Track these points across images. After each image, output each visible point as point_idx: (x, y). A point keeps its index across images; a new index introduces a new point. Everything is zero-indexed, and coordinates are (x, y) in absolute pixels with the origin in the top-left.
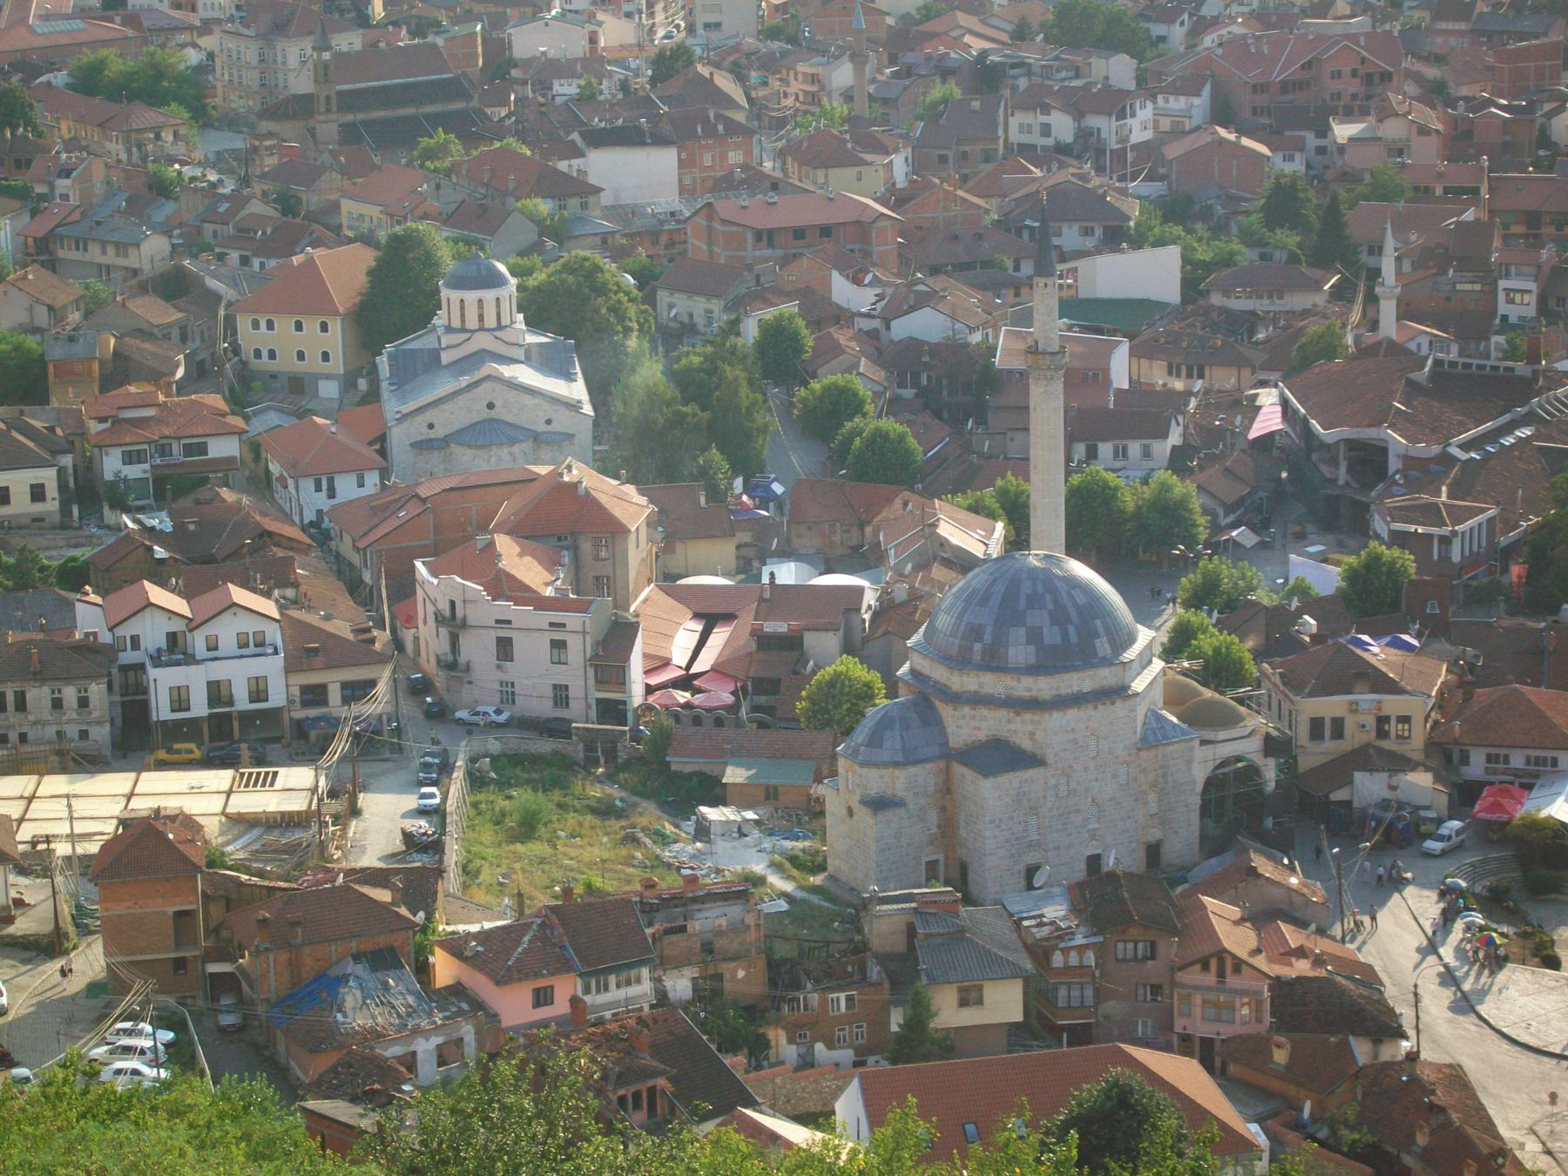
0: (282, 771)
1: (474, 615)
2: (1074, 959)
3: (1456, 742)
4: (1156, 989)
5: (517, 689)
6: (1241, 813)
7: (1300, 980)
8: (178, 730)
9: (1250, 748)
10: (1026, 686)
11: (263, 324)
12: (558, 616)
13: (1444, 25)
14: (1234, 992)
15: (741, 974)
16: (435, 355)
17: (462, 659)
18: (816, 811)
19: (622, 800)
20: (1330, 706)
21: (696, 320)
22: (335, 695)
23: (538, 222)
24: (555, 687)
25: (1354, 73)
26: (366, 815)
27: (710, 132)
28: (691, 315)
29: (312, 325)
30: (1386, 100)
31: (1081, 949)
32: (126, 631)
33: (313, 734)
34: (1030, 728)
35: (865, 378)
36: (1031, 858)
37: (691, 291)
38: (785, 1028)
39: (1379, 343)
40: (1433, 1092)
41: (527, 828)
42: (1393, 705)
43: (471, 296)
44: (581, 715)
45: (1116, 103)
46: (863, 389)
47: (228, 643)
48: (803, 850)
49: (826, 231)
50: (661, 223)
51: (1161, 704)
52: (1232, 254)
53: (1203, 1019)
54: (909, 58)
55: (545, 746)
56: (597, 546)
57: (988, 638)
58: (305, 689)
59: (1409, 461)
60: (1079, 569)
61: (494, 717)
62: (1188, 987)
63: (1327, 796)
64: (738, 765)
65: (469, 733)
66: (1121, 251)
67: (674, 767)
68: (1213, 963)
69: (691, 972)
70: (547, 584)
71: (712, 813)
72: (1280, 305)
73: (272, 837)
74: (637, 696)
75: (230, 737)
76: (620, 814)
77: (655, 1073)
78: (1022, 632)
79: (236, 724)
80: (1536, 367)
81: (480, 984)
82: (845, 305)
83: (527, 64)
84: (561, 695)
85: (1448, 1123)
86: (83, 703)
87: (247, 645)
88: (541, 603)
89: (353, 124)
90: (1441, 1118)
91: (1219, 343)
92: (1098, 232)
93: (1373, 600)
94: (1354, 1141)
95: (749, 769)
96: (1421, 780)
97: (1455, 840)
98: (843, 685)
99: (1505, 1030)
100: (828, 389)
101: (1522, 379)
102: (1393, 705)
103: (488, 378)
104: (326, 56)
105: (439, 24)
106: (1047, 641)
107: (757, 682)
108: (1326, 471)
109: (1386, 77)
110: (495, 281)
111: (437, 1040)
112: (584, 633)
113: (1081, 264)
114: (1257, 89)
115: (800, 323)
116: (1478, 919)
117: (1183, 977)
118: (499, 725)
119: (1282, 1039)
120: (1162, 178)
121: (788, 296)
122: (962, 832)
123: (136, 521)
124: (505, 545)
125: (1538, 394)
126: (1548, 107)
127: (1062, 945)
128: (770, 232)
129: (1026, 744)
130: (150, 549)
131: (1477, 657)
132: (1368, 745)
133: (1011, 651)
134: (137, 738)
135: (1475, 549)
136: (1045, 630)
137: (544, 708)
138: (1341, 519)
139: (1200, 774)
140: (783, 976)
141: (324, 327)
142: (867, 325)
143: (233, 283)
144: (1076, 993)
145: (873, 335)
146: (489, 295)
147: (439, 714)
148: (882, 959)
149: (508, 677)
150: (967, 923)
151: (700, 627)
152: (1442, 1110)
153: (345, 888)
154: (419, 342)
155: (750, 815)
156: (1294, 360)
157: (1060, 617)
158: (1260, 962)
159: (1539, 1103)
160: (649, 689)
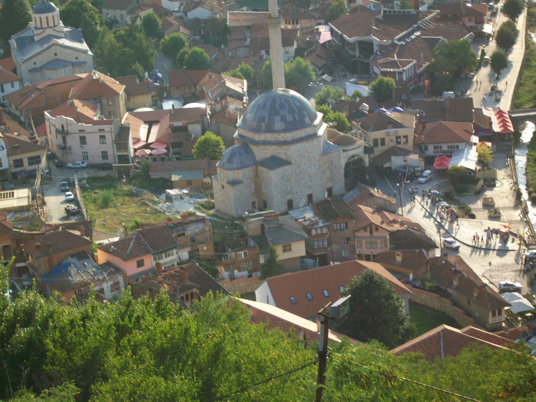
1: (71, 129)
2: (319, 231)
3: (423, 143)
4: (348, 239)
5: (89, 154)
6: (358, 175)
7: (398, 231)
9: (359, 152)
10: (282, 137)
14: (377, 238)
15: (205, 248)
16: (32, 38)
17: (68, 146)
19: (136, 190)
20: (379, 134)
21: (117, 17)
22: (26, 162)
24: (102, 152)
26: (48, 204)
28: (115, 17)
31: (321, 228)
33: (19, 177)
34: (285, 151)
36: (289, 197)
37: (114, 8)
38: (224, 266)
39: (358, 7)
40: (455, 266)
41: (105, 204)
42: (401, 132)
43: (43, 16)
46: (184, 38)
48: (205, 202)
51: (327, 138)
53: (366, 248)
55: (103, 173)
56: (108, 100)
57: (267, 121)
59: (381, 47)
61: (82, 165)
62: (360, 237)
63: (382, 166)
64: (175, 174)
65: (76, 171)
67: (152, 177)
68: (368, 229)
69: (188, 249)
70: (94, 116)
71: (172, 192)
73: (18, 215)
74: (132, 154)
76: (137, 195)
77: (192, 287)
80: (418, 10)
81: (117, 261)
82: (168, 8)
84: (105, 155)
85: (463, 276)
88: (95, 123)
90: (460, 275)
91: (302, 11)
93: (382, 96)
94: (431, 286)
95: (179, 175)
96: (414, 158)
97: (429, 177)
98: (209, 142)
99: (464, 242)
100: (172, 39)
101: (413, 15)
102: (401, 132)
103: (54, 44)
106: (288, 120)
107: (173, 144)
108: (351, 53)
110: (52, 9)
111: (110, 283)
112: (111, 132)
115: (156, 16)
116: (446, 204)
117: (358, 234)
118: (84, 168)
119: (399, 253)
121: (149, 7)
122: (264, 190)
124: (77, 103)
125: (420, 20)
127: (315, 227)
129: (284, 157)
131: (423, 113)
132: (394, 147)
133: (276, 125)
135: (410, 75)
136: (287, 116)
139: (343, 162)
140: (220, 248)
144: (321, 243)
145: (181, 18)
146: (50, 15)
147: (61, 166)
148: (254, 238)
149: (85, 150)
150: (282, 222)
152: (460, 272)
153: (64, 232)
155: (185, 191)
157: (291, 111)
158: (384, 226)
159: (483, 266)
160: (135, 150)
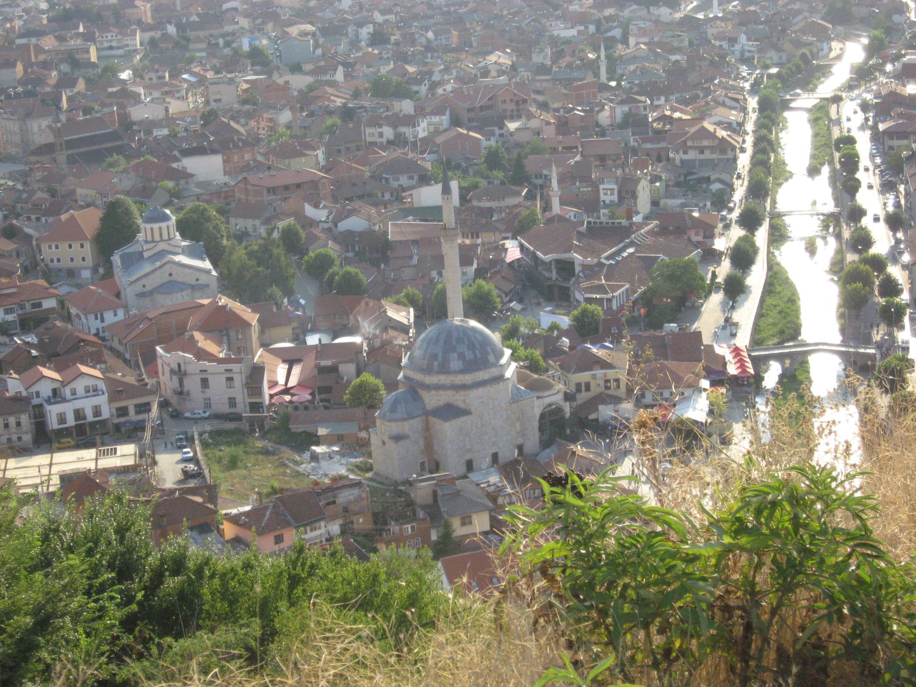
0: (119, 448)
1: (190, 369)
8: (61, 433)
9: (558, 398)
11: (54, 247)
12: (229, 366)
13: (540, 78)
15: (361, 520)
16: (141, 254)
17: (185, 390)
18: (366, 444)
20: (584, 377)
22: (132, 410)
23: (169, 191)
25: (511, 100)
26: (159, 464)
27: (236, 146)
29: (76, 245)
30: (529, 111)
32: (34, 389)
33: (123, 430)
34: (463, 398)
35: (332, 249)
41: (233, 463)
42: (611, 374)
43: (156, 226)
44: (241, 407)
45: (411, 121)
47: (81, 391)
49: (298, 186)
50: (221, 188)
52: (477, 183)
54: (313, 107)
55: (231, 426)
56: (237, 332)
58: (118, 409)
59: (585, 267)
60: (473, 323)
61: (203, 415)
64: (322, 427)
65: (196, 423)
66: (431, 185)
71: (318, 449)
72: (503, 204)
73: (122, 477)
75: (84, 434)
78: (455, 355)
79: (88, 428)
83: (140, 123)
84: (232, 402)
86: (18, 424)
87: (89, 391)
89: (73, 155)
92: (416, 177)
93: (586, 328)
95: (327, 428)
100: (317, 256)
101: (625, 227)
102: (611, 374)
103: (168, 262)
104: (59, 125)
105: (93, 109)
106: (467, 358)
108: (547, 274)
109: (525, 101)
110: (166, 218)
112: (241, 373)
113: (414, 192)
114: (470, 110)
118: (206, 418)
120: (434, 152)
121: (288, 216)
122: (435, 448)
123: (20, 339)
124: (198, 335)
125: (634, 233)
126: (596, 109)
128: (274, 188)
129: (461, 405)
130: (29, 352)
134: (45, 439)
137: (226, 409)
138: (560, 296)
139: (538, 412)
140: (380, 520)
141: (82, 246)
142: (326, 226)
143: (36, 229)
146: (164, 225)
147: (176, 415)
148: (424, 507)
149: (207, 396)
151: (287, 367)
154: (130, 249)
155: (336, 449)
156: (518, 229)
157: (472, 347)
160: (271, 396)
